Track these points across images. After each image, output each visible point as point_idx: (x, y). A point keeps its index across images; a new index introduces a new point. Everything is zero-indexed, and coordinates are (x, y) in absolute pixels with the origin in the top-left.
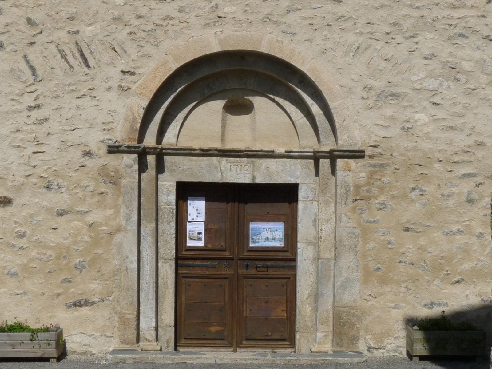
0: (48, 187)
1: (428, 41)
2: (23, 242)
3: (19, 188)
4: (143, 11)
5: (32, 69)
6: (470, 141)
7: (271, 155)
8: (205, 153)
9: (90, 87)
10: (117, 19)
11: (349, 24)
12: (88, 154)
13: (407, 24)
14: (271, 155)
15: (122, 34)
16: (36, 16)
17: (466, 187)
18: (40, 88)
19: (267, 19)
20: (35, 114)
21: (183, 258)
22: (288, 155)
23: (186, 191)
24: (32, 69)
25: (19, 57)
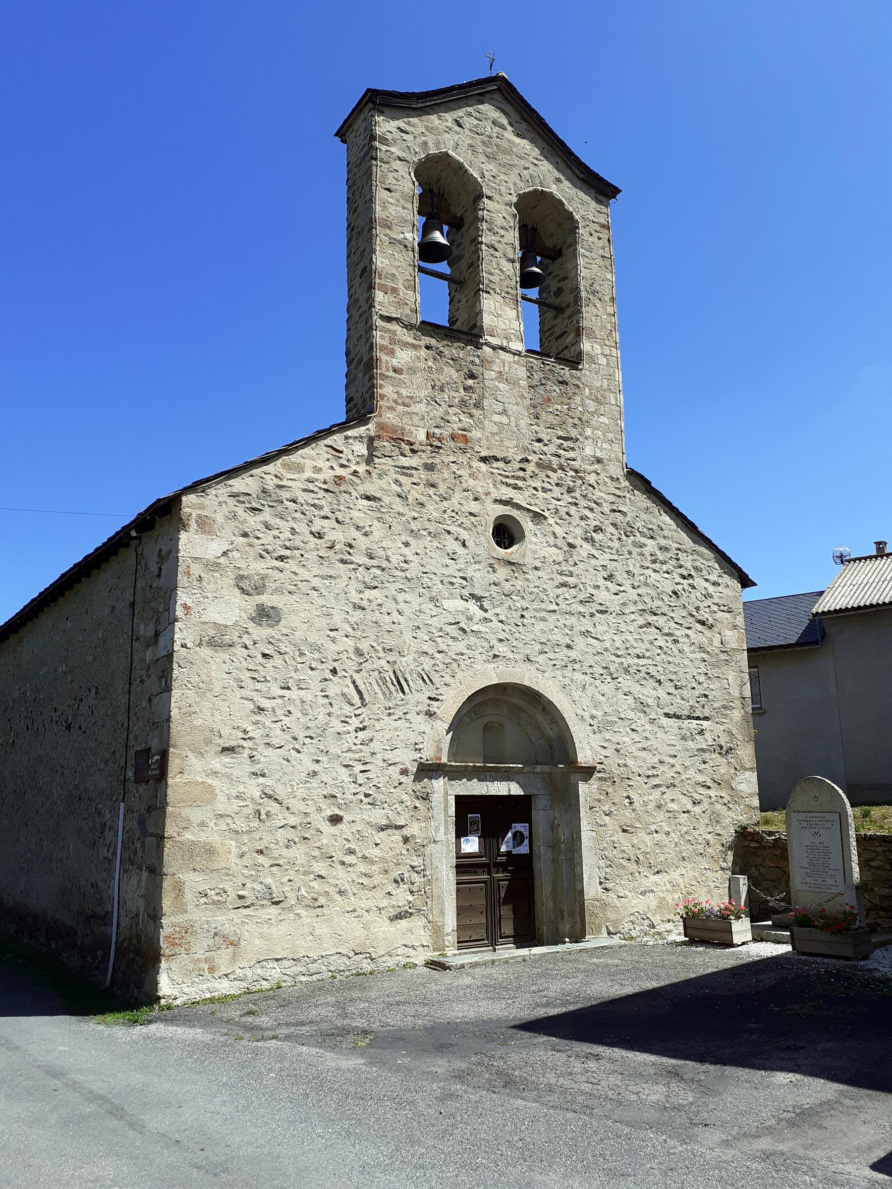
1: (627, 683)
4: (443, 647)
5: (359, 692)
9: (405, 711)
11: (577, 666)
16: (364, 646)
20: (361, 734)
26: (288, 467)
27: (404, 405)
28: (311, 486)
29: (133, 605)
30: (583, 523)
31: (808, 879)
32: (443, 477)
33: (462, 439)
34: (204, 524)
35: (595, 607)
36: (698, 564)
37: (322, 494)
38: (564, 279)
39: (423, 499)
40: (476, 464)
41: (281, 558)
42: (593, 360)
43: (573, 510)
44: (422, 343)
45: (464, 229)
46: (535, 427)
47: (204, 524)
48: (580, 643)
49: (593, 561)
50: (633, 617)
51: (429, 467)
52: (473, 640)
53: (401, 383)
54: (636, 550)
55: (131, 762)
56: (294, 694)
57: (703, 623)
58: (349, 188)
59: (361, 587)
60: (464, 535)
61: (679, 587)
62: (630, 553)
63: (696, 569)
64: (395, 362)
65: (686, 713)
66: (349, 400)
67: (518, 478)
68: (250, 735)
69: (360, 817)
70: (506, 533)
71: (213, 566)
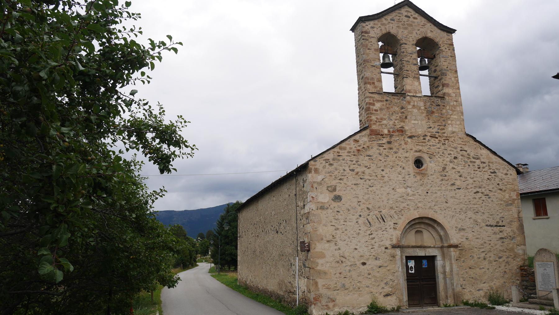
0: (376, 259)
2: (370, 276)
3: (368, 259)
4: (398, 205)
5: (369, 222)
6: (483, 242)
7: (430, 247)
8: (413, 247)
10: (392, 208)
11: (450, 209)
12: (386, 248)
13: (464, 209)
14: (430, 247)
15: (392, 212)
16: (370, 207)
17: (483, 254)
18: (372, 228)
19: (430, 208)
20: (371, 236)
21: (408, 275)
22: (434, 247)
23: (408, 258)
24: (369, 222)
25: (366, 219)
26: (341, 148)
27: (379, 122)
28: (349, 154)
29: (296, 195)
30: (449, 156)
31: (542, 286)
32: (395, 145)
33: (401, 131)
34: (316, 171)
35: (456, 187)
36: (497, 167)
37: (353, 156)
38: (437, 66)
39: (387, 154)
40: (407, 139)
41: (340, 179)
42: (449, 95)
43: (445, 152)
44: (384, 100)
45: (397, 56)
46: (428, 123)
47: (316, 171)
48: (451, 201)
49: (454, 170)
50: (471, 190)
51: (389, 143)
52: (409, 202)
53: (377, 114)
54: (471, 164)
55: (299, 245)
56: (348, 223)
57: (501, 190)
58: (356, 48)
59: (368, 187)
60: (404, 165)
61: (490, 177)
62: (469, 166)
63: (497, 169)
64: (375, 108)
65: (495, 224)
66: (360, 121)
67: (423, 142)
68: (328, 174)
69: (372, 263)
70: (418, 163)
71: (320, 184)
